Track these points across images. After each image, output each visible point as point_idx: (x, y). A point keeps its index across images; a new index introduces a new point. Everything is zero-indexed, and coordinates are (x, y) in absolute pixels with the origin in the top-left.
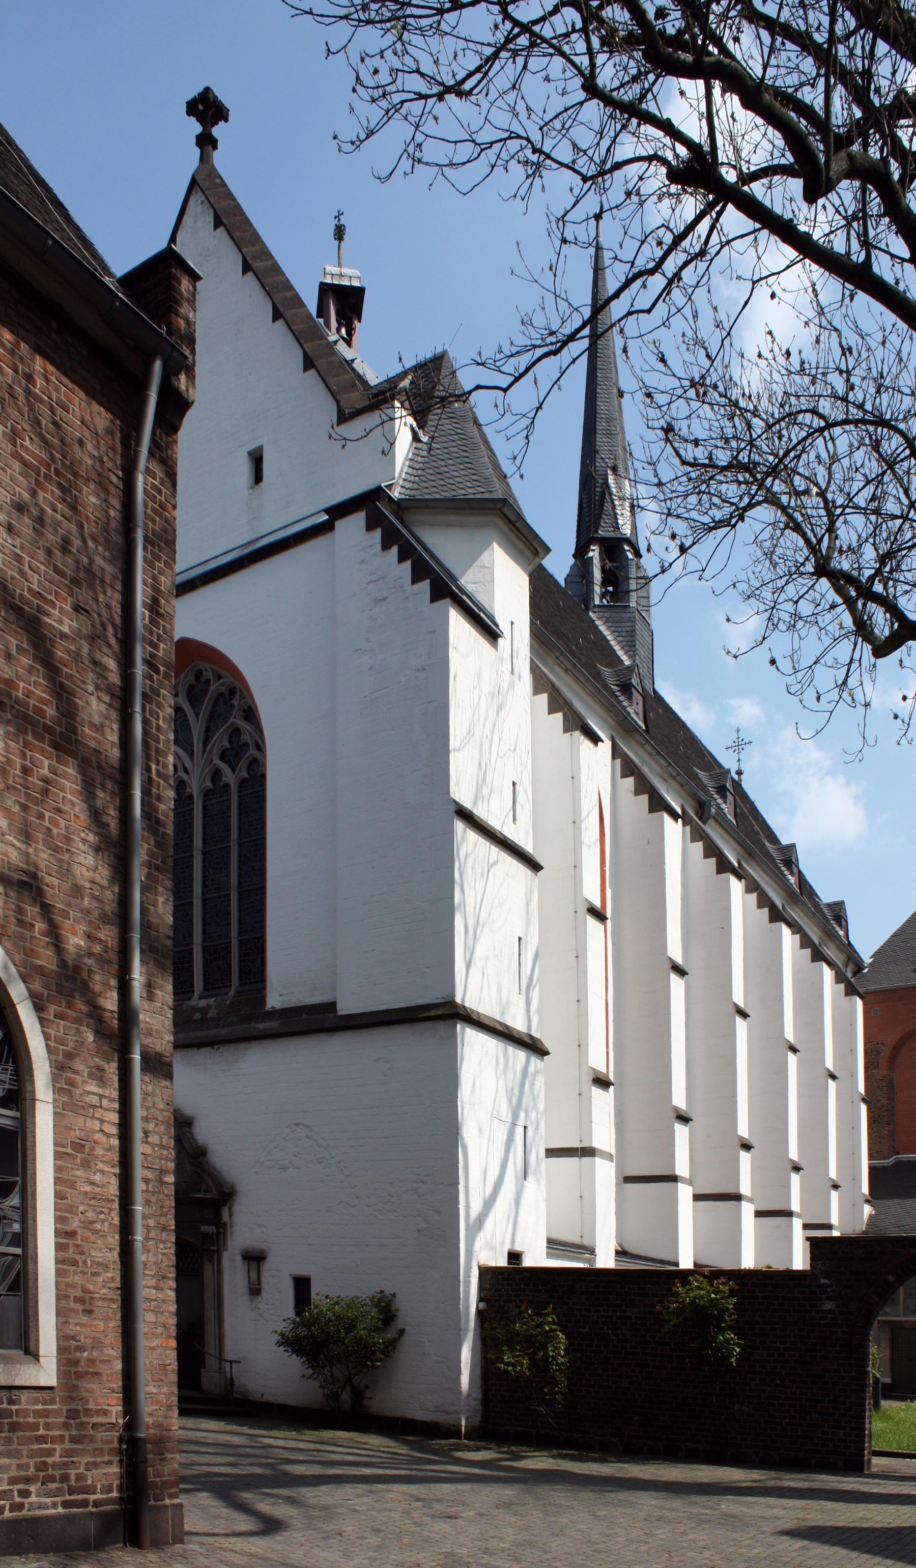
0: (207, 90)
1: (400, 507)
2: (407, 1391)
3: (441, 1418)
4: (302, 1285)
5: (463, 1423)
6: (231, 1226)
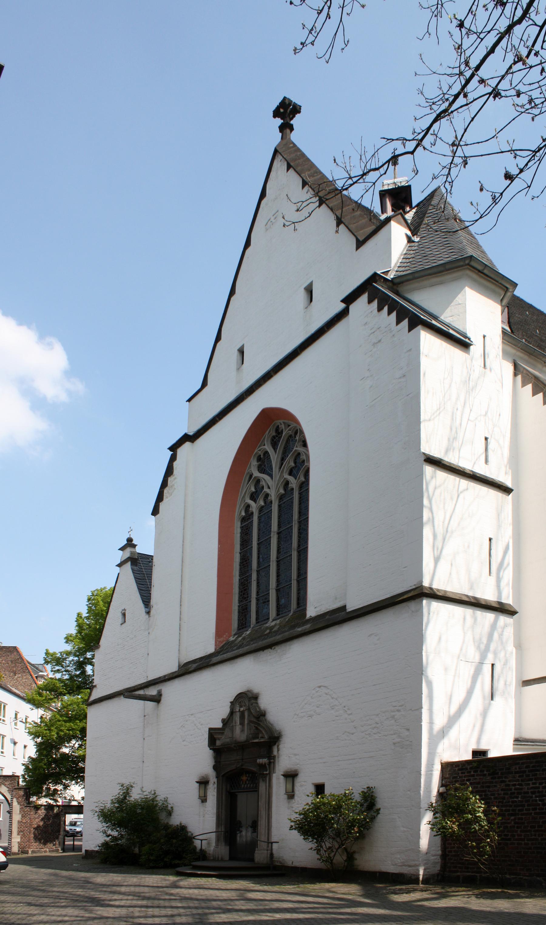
0: (285, 98)
1: (396, 284)
2: (382, 854)
3: (405, 870)
4: (320, 789)
5: (421, 872)
6: (278, 757)
